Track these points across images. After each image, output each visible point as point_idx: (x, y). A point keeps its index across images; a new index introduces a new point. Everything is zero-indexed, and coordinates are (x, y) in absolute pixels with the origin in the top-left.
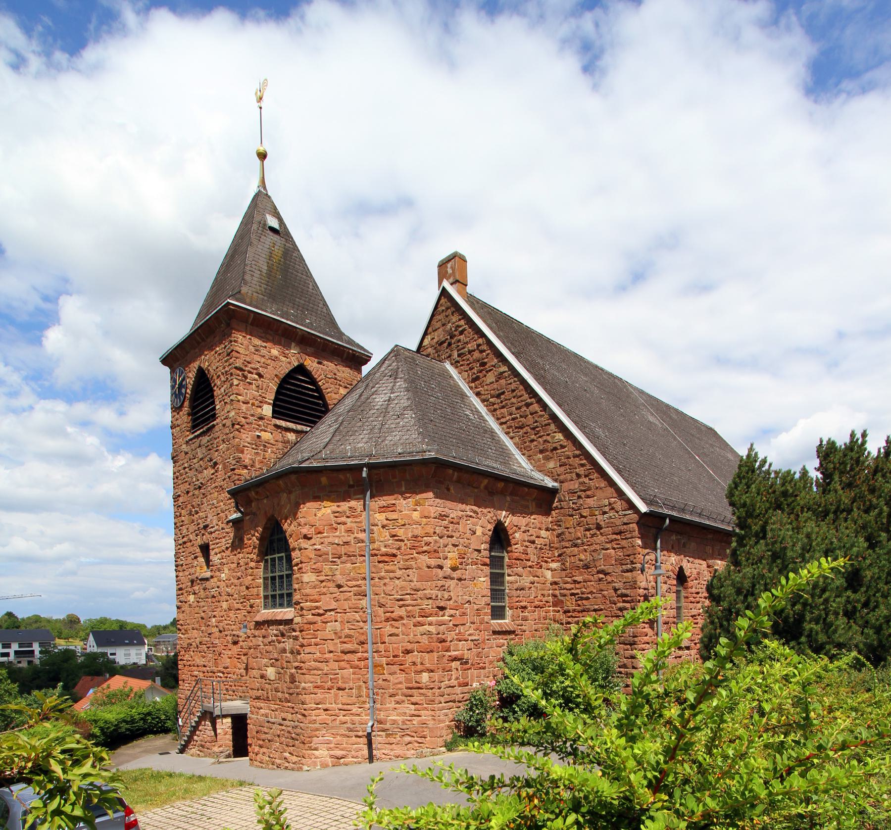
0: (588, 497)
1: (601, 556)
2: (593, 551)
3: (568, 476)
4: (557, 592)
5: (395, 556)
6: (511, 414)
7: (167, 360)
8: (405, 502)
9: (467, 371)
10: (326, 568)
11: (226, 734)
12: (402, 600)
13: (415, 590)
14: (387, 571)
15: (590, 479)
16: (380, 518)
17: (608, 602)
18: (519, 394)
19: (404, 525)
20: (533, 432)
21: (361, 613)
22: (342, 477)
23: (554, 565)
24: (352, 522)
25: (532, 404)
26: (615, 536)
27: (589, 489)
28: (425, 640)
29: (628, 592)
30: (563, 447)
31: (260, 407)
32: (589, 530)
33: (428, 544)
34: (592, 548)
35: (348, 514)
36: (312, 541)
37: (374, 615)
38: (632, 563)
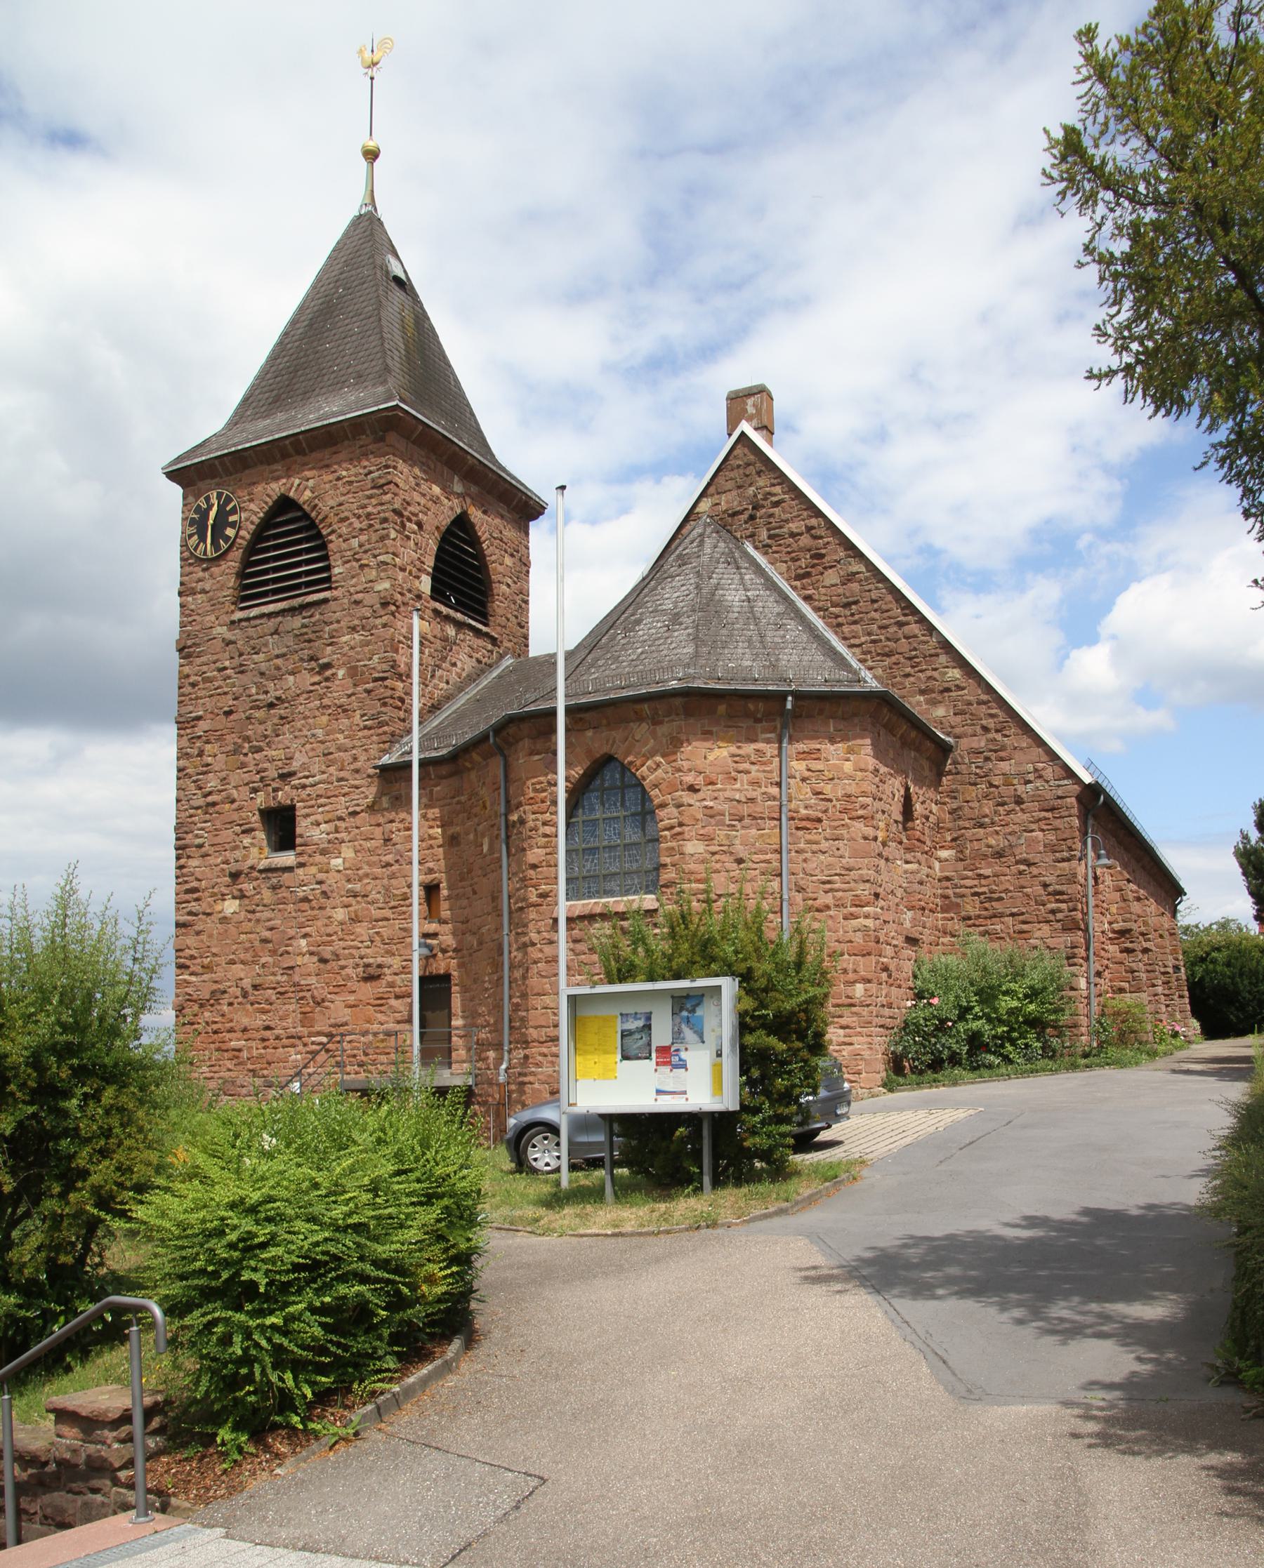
0: (1002, 759)
1: (1022, 841)
2: (1010, 834)
3: (969, 730)
4: (950, 892)
5: (819, 820)
6: (869, 634)
7: (187, 474)
8: (832, 748)
9: (786, 562)
10: (721, 834)
12: (829, 882)
14: (809, 842)
15: (1006, 736)
16: (799, 767)
17: (1032, 903)
18: (884, 607)
19: (832, 779)
20: (909, 663)
21: (770, 901)
22: (751, 706)
23: (944, 854)
24: (758, 771)
25: (908, 624)
27: (1003, 748)
28: (858, 938)
29: (1063, 888)
31: (418, 577)
32: (1002, 804)
33: (864, 807)
34: (1008, 829)
35: (752, 759)
36: (700, 795)
38: (1071, 849)
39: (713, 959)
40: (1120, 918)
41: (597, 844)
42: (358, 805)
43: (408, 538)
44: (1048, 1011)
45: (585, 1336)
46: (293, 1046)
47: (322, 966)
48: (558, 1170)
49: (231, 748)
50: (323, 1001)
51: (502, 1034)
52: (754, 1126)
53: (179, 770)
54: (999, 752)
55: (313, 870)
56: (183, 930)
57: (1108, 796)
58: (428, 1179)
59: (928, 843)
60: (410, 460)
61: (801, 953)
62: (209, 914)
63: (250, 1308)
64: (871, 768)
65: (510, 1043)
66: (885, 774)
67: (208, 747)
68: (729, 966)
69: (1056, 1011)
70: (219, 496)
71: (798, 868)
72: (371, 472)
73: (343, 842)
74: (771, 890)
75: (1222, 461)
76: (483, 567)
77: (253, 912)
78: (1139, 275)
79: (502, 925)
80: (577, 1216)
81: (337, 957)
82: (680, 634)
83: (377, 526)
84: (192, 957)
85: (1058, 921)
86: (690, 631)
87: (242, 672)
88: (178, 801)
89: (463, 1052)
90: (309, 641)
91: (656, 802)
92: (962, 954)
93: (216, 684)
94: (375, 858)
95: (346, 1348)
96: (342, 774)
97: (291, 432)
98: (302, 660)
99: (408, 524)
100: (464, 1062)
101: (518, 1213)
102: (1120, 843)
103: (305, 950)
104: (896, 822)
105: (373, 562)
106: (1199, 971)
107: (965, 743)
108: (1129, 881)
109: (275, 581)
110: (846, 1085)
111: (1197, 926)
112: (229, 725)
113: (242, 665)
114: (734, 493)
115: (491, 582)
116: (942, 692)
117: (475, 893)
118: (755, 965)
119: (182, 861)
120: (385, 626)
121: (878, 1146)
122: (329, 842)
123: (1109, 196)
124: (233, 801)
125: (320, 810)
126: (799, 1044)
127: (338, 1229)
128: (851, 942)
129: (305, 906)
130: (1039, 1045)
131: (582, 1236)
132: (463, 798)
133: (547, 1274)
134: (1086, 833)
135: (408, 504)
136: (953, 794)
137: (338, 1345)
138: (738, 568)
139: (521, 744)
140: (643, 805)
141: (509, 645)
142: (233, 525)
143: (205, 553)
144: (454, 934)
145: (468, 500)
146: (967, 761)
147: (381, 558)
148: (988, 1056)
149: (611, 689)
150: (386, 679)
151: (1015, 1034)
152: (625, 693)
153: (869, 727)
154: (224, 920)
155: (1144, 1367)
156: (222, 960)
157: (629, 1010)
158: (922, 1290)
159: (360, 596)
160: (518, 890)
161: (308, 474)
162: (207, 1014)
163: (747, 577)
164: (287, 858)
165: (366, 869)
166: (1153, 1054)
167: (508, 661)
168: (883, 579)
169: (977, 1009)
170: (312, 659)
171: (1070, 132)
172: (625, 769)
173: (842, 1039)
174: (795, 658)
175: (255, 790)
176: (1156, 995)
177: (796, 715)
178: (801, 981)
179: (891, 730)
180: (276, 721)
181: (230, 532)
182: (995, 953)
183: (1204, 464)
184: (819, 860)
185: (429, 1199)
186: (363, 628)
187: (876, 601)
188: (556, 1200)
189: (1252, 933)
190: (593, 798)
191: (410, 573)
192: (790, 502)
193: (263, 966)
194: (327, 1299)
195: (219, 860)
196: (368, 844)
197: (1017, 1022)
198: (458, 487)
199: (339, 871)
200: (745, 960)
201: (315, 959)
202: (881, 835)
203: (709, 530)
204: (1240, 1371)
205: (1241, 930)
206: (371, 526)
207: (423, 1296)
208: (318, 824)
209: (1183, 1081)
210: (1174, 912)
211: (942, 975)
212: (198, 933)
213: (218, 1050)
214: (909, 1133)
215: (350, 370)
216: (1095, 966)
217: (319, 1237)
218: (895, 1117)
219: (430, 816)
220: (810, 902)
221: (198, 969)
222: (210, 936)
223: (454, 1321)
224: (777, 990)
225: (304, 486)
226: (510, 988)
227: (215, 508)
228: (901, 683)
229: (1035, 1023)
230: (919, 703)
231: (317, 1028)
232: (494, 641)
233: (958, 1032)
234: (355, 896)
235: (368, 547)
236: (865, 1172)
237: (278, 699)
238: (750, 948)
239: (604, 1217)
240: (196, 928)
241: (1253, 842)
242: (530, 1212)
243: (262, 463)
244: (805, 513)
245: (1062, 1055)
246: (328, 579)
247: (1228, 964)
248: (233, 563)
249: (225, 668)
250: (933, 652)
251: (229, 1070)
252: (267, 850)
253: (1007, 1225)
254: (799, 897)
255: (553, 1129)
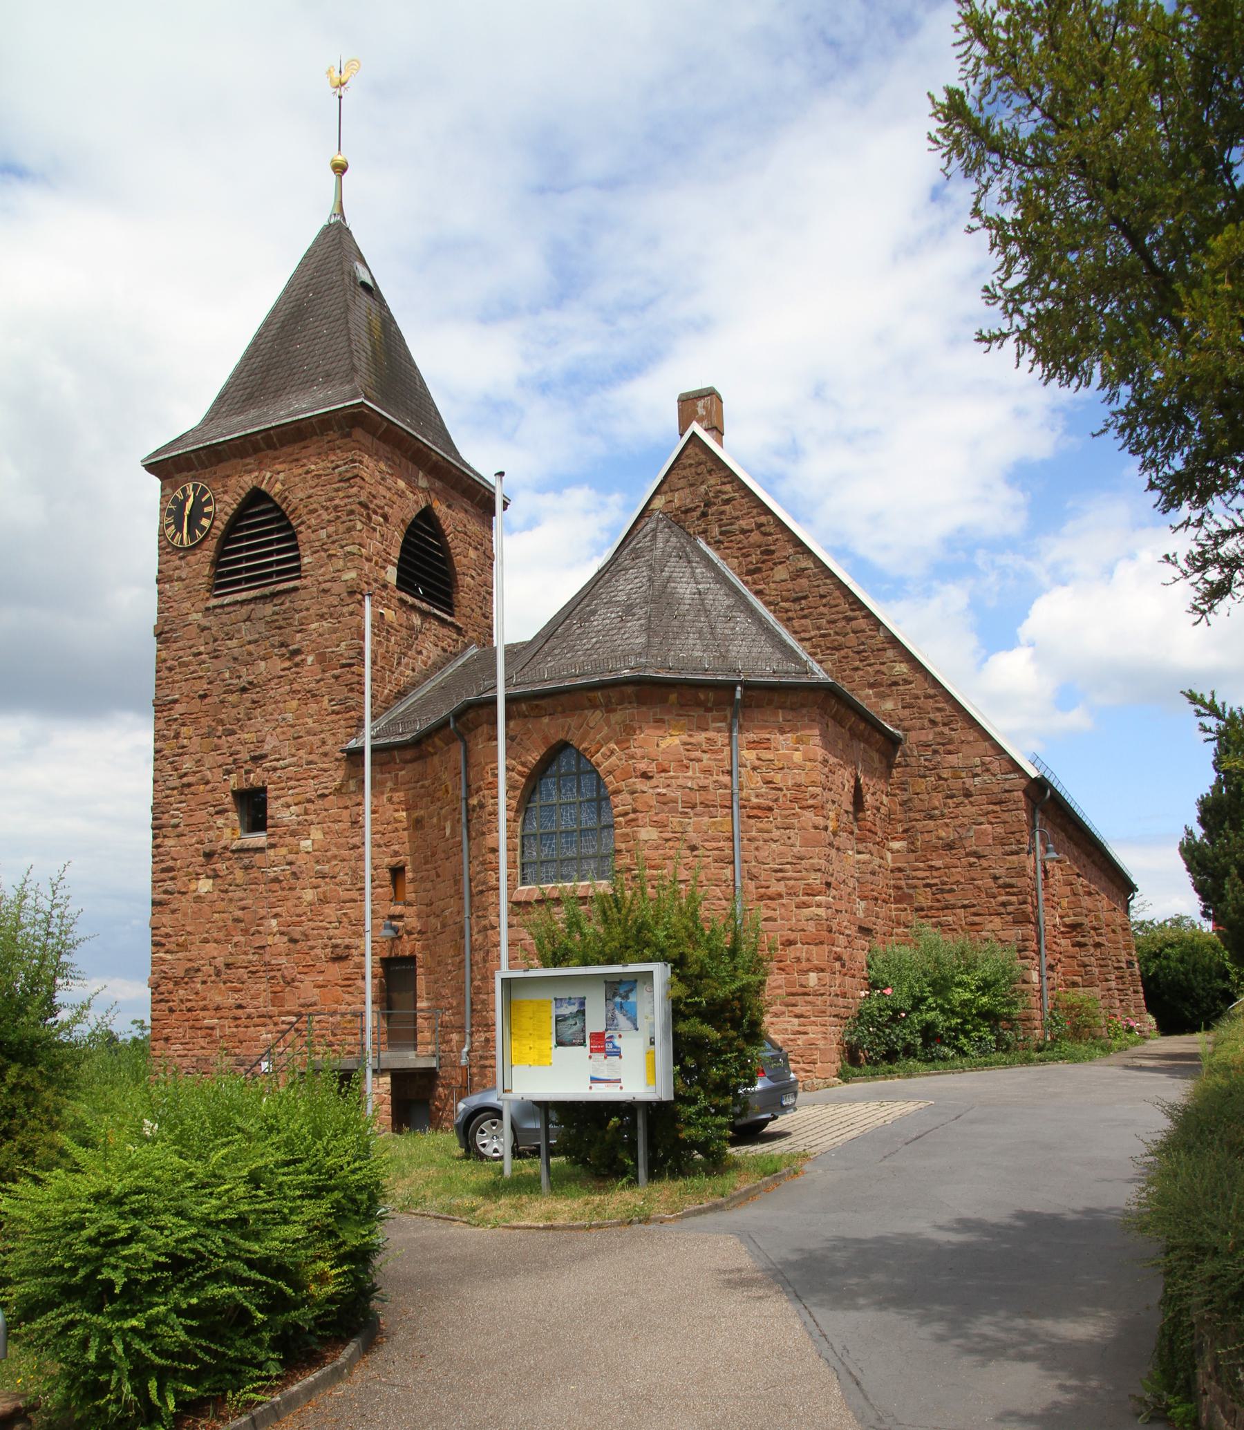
0: (950, 753)
1: (971, 834)
3: (918, 723)
4: (903, 883)
5: (770, 809)
6: (819, 628)
7: (165, 467)
10: (675, 821)
11: (382, 1103)
12: (781, 871)
13: (799, 858)
14: (760, 830)
16: (749, 756)
17: (983, 895)
18: (832, 602)
20: (857, 656)
23: (896, 845)
24: (710, 759)
25: (855, 619)
26: (992, 807)
27: (951, 742)
28: (811, 927)
29: (1013, 881)
30: (907, 682)
31: (384, 568)
32: (952, 797)
33: (814, 796)
34: (957, 822)
35: (704, 747)
36: (654, 782)
37: (744, 890)
38: (1019, 842)
39: (647, 944)
40: (1071, 912)
41: (554, 829)
42: (326, 788)
43: (375, 530)
44: (1001, 1003)
45: (490, 1341)
46: (264, 1025)
47: (292, 946)
48: (501, 1158)
49: (205, 730)
50: (293, 980)
51: (464, 1017)
52: (690, 1117)
53: (157, 752)
54: (947, 745)
55: (284, 851)
56: (159, 908)
57: (1054, 791)
58: (319, 1170)
59: (880, 834)
60: (376, 455)
61: (736, 939)
62: (184, 893)
63: (109, 1309)
64: (820, 758)
65: (472, 1026)
66: (835, 765)
67: (184, 729)
68: (662, 951)
69: (1009, 1004)
70: (195, 488)
71: (750, 856)
72: (338, 466)
73: (312, 824)
74: (724, 878)
75: (1122, 429)
76: (448, 560)
77: (226, 891)
78: (1031, 239)
79: (463, 907)
80: (513, 1206)
81: (307, 937)
82: (634, 625)
83: (345, 518)
84: (168, 935)
85: (1009, 914)
86: (642, 621)
87: (216, 657)
88: (155, 782)
89: (427, 1034)
90: (280, 628)
91: (611, 788)
92: (920, 945)
93: (192, 668)
94: (343, 840)
95: (214, 1354)
96: (311, 757)
97: (262, 428)
98: (273, 646)
99: (374, 517)
100: (429, 1044)
101: (458, 1201)
102: (1070, 838)
103: (275, 930)
104: (847, 812)
105: (340, 553)
106: (1153, 967)
107: (913, 736)
108: (1079, 875)
109: (248, 569)
110: (792, 1075)
111: (1151, 923)
112: (204, 708)
113: (216, 650)
114: (687, 491)
115: (456, 574)
116: (890, 685)
117: (438, 876)
118: (688, 951)
119: (159, 841)
120: (351, 614)
121: (824, 1139)
122: (299, 824)
123: (995, 158)
124: (207, 783)
125: (291, 792)
126: (733, 1033)
127: (209, 1224)
128: (803, 930)
129: (276, 886)
130: (993, 1038)
131: (514, 1228)
132: (427, 783)
133: (472, 1269)
134: (1034, 827)
135: (374, 497)
136: (903, 786)
137: (207, 1350)
138: (689, 562)
139: (480, 729)
140: (598, 792)
141: (474, 635)
142: (208, 516)
143: (182, 543)
144: (419, 916)
145: (433, 495)
146: (916, 753)
147: (348, 549)
148: (943, 1048)
149: (566, 677)
150: (352, 665)
151: (969, 1027)
152: (579, 681)
153: (818, 718)
154: (198, 899)
155: (1068, 1396)
156: (196, 939)
157: (564, 994)
158: (843, 1299)
159: (328, 585)
160: (480, 872)
161: (278, 467)
162: (181, 992)
163: (698, 571)
164: (259, 839)
165: (334, 851)
166: (1107, 1049)
167: (473, 651)
168: (832, 575)
169: (930, 1000)
170: (282, 645)
171: (952, 93)
172: (580, 755)
173: (797, 1028)
174: (744, 649)
175: (228, 772)
176: (1109, 990)
177: (746, 704)
178: (735, 968)
179: (840, 722)
180: (248, 705)
181: (205, 522)
182: (948, 945)
183: (1103, 431)
184: (774, 847)
185: (317, 1192)
186: (331, 615)
187: (825, 597)
188: (494, 1190)
189: (1205, 930)
190: (549, 784)
191: (376, 563)
192: (740, 501)
193: (236, 945)
194: (194, 1301)
195: (194, 840)
196: (336, 827)
197: (970, 1014)
198: (423, 482)
199: (308, 853)
200: (677, 945)
201: (286, 939)
202: (831, 825)
203: (661, 526)
204: (1169, 1407)
205: (1194, 927)
206: (339, 517)
207: (312, 1296)
208: (289, 806)
209: (1136, 1077)
210: (1127, 909)
211: (895, 966)
212: (173, 912)
213: (192, 1027)
214: (857, 1125)
215: (319, 369)
216: (1047, 960)
217: (186, 1233)
218: (847, 1109)
219: (395, 799)
220: (762, 890)
221: (173, 947)
222: (185, 915)
223: (353, 1319)
224: (710, 977)
225: (275, 478)
226: (472, 971)
227: (191, 500)
228: (851, 677)
229: (988, 1015)
230: (868, 697)
231: (287, 1008)
232: (459, 630)
233: (912, 1022)
234: (323, 877)
235: (335, 538)
236: (807, 1167)
237: (250, 683)
238: (683, 933)
239: (540, 1208)
240: (172, 906)
241: (1198, 839)
242: (468, 1201)
243: (235, 457)
244: (755, 511)
245: (1016, 1049)
246: (298, 569)
247: (1181, 961)
248: (208, 552)
249: (200, 654)
250: (880, 646)
251: (203, 1048)
252: (239, 831)
253: (941, 1228)
254: (752, 885)
255: (497, 1113)
